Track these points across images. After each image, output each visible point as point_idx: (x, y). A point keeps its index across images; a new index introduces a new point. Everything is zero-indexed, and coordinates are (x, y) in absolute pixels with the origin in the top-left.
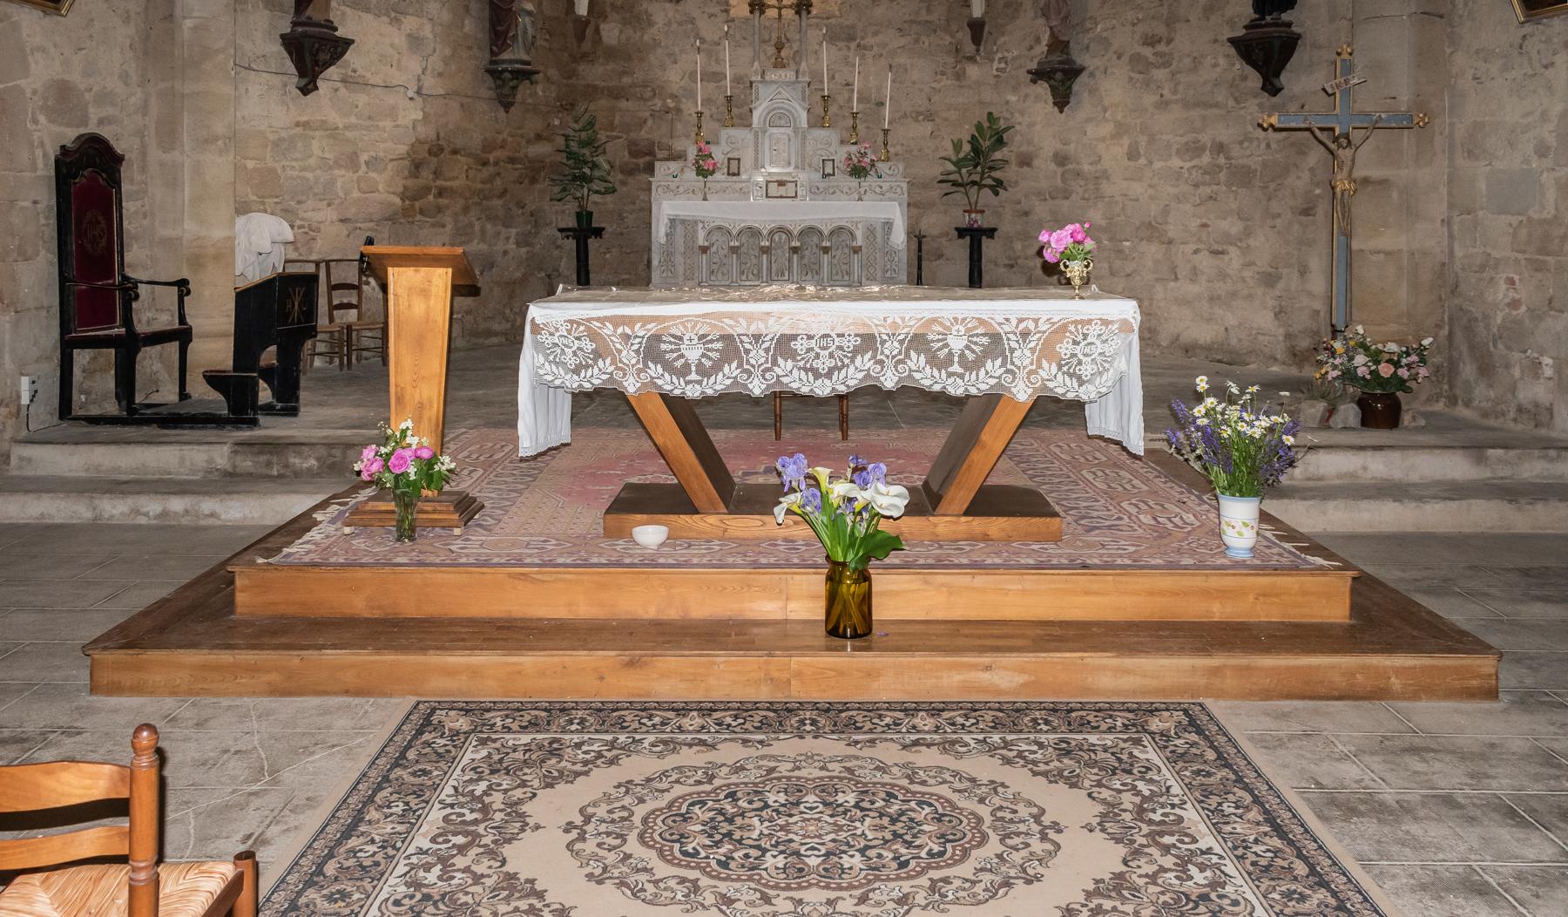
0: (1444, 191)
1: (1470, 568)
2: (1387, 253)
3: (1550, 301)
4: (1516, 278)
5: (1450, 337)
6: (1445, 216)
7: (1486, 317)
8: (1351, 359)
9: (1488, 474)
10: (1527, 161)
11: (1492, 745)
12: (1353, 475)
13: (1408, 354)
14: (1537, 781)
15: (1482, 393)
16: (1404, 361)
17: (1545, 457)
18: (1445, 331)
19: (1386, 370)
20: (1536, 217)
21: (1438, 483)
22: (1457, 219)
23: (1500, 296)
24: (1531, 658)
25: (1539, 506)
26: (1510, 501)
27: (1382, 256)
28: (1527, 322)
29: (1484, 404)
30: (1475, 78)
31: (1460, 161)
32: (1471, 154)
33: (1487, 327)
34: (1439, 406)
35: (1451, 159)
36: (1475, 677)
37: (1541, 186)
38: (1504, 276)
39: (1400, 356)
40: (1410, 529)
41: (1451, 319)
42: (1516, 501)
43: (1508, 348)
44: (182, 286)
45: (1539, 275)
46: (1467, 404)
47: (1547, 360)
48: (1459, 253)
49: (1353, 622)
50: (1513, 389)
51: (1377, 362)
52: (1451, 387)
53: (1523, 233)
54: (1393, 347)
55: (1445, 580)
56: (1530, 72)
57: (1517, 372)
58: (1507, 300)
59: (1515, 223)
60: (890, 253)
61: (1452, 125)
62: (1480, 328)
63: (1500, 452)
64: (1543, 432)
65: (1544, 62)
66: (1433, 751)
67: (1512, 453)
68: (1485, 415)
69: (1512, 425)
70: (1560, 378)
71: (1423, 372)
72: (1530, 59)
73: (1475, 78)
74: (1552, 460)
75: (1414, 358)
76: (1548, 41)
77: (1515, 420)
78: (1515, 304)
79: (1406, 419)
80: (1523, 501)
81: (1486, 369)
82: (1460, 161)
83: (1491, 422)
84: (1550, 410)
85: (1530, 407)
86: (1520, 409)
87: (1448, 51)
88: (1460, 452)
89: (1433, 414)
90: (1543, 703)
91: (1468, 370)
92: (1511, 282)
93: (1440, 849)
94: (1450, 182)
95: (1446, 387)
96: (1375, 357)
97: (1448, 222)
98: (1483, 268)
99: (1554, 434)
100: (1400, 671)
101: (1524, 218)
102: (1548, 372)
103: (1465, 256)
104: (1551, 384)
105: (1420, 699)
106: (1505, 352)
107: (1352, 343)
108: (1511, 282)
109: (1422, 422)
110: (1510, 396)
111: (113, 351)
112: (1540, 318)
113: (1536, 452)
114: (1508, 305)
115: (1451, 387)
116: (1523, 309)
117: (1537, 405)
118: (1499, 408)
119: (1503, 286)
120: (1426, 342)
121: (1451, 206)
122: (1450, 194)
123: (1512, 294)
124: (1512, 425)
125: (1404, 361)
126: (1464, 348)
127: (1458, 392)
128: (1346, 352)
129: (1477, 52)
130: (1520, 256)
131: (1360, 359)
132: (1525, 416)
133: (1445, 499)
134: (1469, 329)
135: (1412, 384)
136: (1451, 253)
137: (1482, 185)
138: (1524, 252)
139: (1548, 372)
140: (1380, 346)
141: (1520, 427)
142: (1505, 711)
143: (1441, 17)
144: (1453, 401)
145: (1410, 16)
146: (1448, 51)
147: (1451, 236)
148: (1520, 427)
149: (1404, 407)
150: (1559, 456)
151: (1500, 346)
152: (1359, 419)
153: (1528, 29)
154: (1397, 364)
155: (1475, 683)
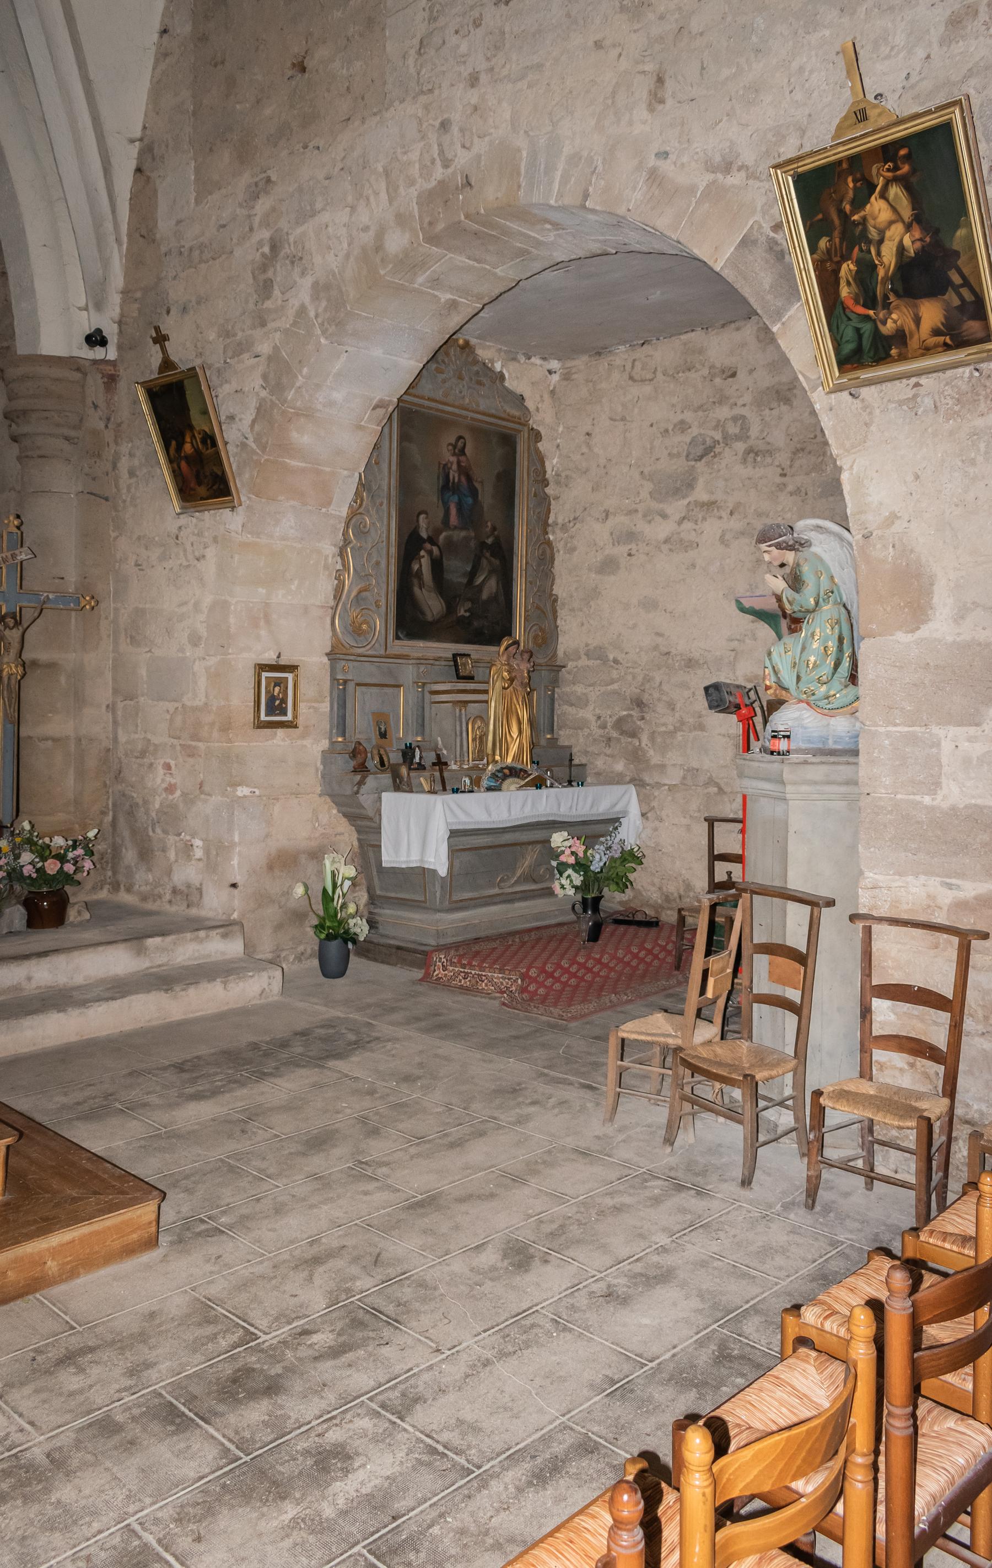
0: (109, 675)
1: (130, 1074)
2: (55, 740)
3: (201, 785)
4: (172, 763)
5: (114, 823)
6: (110, 702)
7: (146, 802)
8: (17, 857)
9: (147, 964)
10: (182, 650)
11: (152, 1315)
12: (17, 988)
13: (74, 847)
14: (195, 1351)
15: (143, 878)
16: (70, 855)
17: (196, 939)
18: (109, 818)
19: (52, 867)
20: (189, 704)
21: (102, 981)
22: (120, 705)
23: (159, 781)
24: (187, 1177)
25: (192, 991)
26: (166, 991)
27: (50, 743)
28: (181, 806)
29: (143, 888)
30: (137, 565)
31: (124, 647)
32: (133, 641)
33: (147, 813)
34: (103, 894)
35: (116, 643)
36: (133, 1232)
37: (194, 674)
38: (162, 761)
39: (67, 850)
40: (73, 1038)
41: (114, 805)
42: (171, 989)
43: (165, 832)
44: (658, 634)
45: (191, 760)
46: (129, 890)
47: (198, 842)
48: (122, 738)
49: (8, 1197)
50: (169, 872)
51: (44, 859)
52: (115, 873)
53: (179, 720)
54: (59, 841)
55: (107, 1096)
56: (185, 563)
57: (172, 855)
58: (164, 786)
59: (172, 710)
60: (523, 344)
61: (116, 610)
62: (140, 813)
63: (158, 940)
64: (194, 912)
65: (197, 554)
66: (92, 1350)
67: (169, 939)
68: (144, 899)
69: (167, 907)
70: (208, 858)
71: (88, 865)
72: (185, 551)
73: (137, 565)
74: (201, 941)
75: (80, 851)
76: (200, 534)
77: (170, 902)
78: (170, 789)
79: (72, 914)
80: (177, 988)
81: (145, 854)
82: (124, 647)
83: (150, 906)
84: (200, 890)
85: (183, 888)
86: (175, 891)
87: (113, 535)
88: (121, 946)
89: (99, 903)
90: (199, 1234)
91: (129, 855)
92: (168, 767)
93: (95, 1513)
94: (115, 668)
95: (109, 873)
96: (43, 852)
97: (111, 708)
98: (143, 754)
99: (203, 913)
100: (54, 1252)
101: (179, 705)
102: (199, 853)
103: (127, 742)
104: (201, 864)
105: (78, 1275)
106: (162, 835)
107: (18, 840)
108: (168, 767)
109: (87, 916)
110: (166, 879)
111: (19, 352)
112: (192, 802)
113: (189, 935)
114: (166, 789)
115: (115, 873)
116: (178, 793)
117: (189, 886)
118: (156, 892)
119: (161, 771)
120: (91, 834)
121: (116, 691)
122: (114, 680)
123: (168, 779)
124: (167, 907)
125: (70, 855)
126: (126, 834)
127: (121, 878)
128: (13, 850)
129: (139, 538)
130: (175, 742)
131: (26, 857)
132: (179, 897)
133: (107, 999)
134: (131, 813)
135: (78, 877)
136: (115, 739)
137: (143, 672)
138: (179, 738)
139: (199, 853)
140: (47, 840)
141: (173, 909)
142: (165, 1258)
143: (107, 499)
144: (116, 887)
145: (78, 494)
146: (113, 535)
147: (115, 722)
148: (173, 909)
149: (72, 900)
150: (207, 936)
151: (158, 830)
152: (24, 922)
153: (184, 520)
154: (62, 858)
155: (135, 1236)
